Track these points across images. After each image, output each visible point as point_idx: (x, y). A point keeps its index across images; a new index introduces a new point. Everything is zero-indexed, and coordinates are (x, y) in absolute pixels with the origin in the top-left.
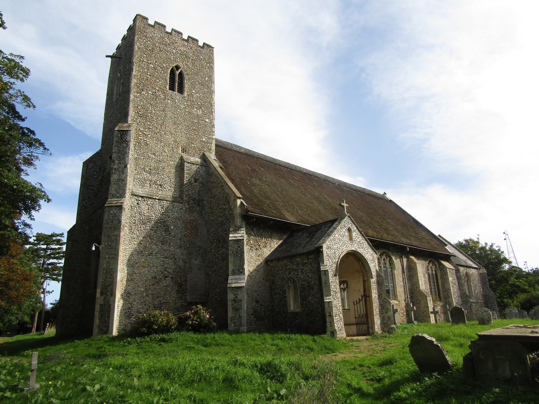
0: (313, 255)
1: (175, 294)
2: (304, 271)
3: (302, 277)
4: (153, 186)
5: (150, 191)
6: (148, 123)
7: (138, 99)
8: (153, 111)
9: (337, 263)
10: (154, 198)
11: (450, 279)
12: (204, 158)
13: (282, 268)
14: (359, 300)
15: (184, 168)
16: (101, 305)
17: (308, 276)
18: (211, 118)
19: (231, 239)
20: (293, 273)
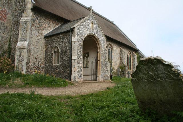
3: (62, 46)
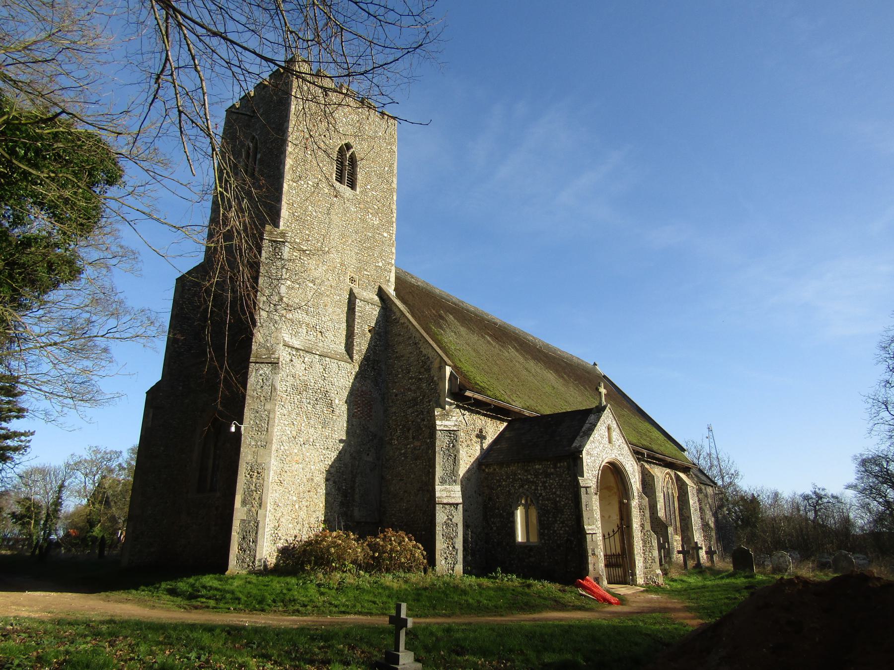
0: (565, 463)
1: (338, 508)
2: (547, 485)
4: (311, 333)
5: (307, 341)
6: (307, 232)
7: (294, 192)
8: (314, 213)
9: (598, 477)
10: (314, 352)
11: (691, 502)
12: (381, 293)
13: (508, 477)
14: (613, 531)
15: (354, 308)
16: (243, 521)
17: (555, 493)
18: (391, 232)
19: (440, 428)
20: (527, 486)
